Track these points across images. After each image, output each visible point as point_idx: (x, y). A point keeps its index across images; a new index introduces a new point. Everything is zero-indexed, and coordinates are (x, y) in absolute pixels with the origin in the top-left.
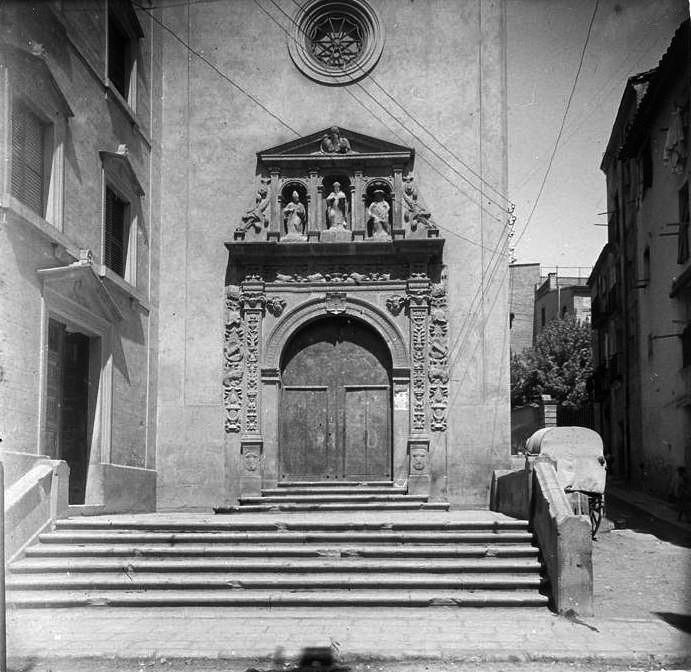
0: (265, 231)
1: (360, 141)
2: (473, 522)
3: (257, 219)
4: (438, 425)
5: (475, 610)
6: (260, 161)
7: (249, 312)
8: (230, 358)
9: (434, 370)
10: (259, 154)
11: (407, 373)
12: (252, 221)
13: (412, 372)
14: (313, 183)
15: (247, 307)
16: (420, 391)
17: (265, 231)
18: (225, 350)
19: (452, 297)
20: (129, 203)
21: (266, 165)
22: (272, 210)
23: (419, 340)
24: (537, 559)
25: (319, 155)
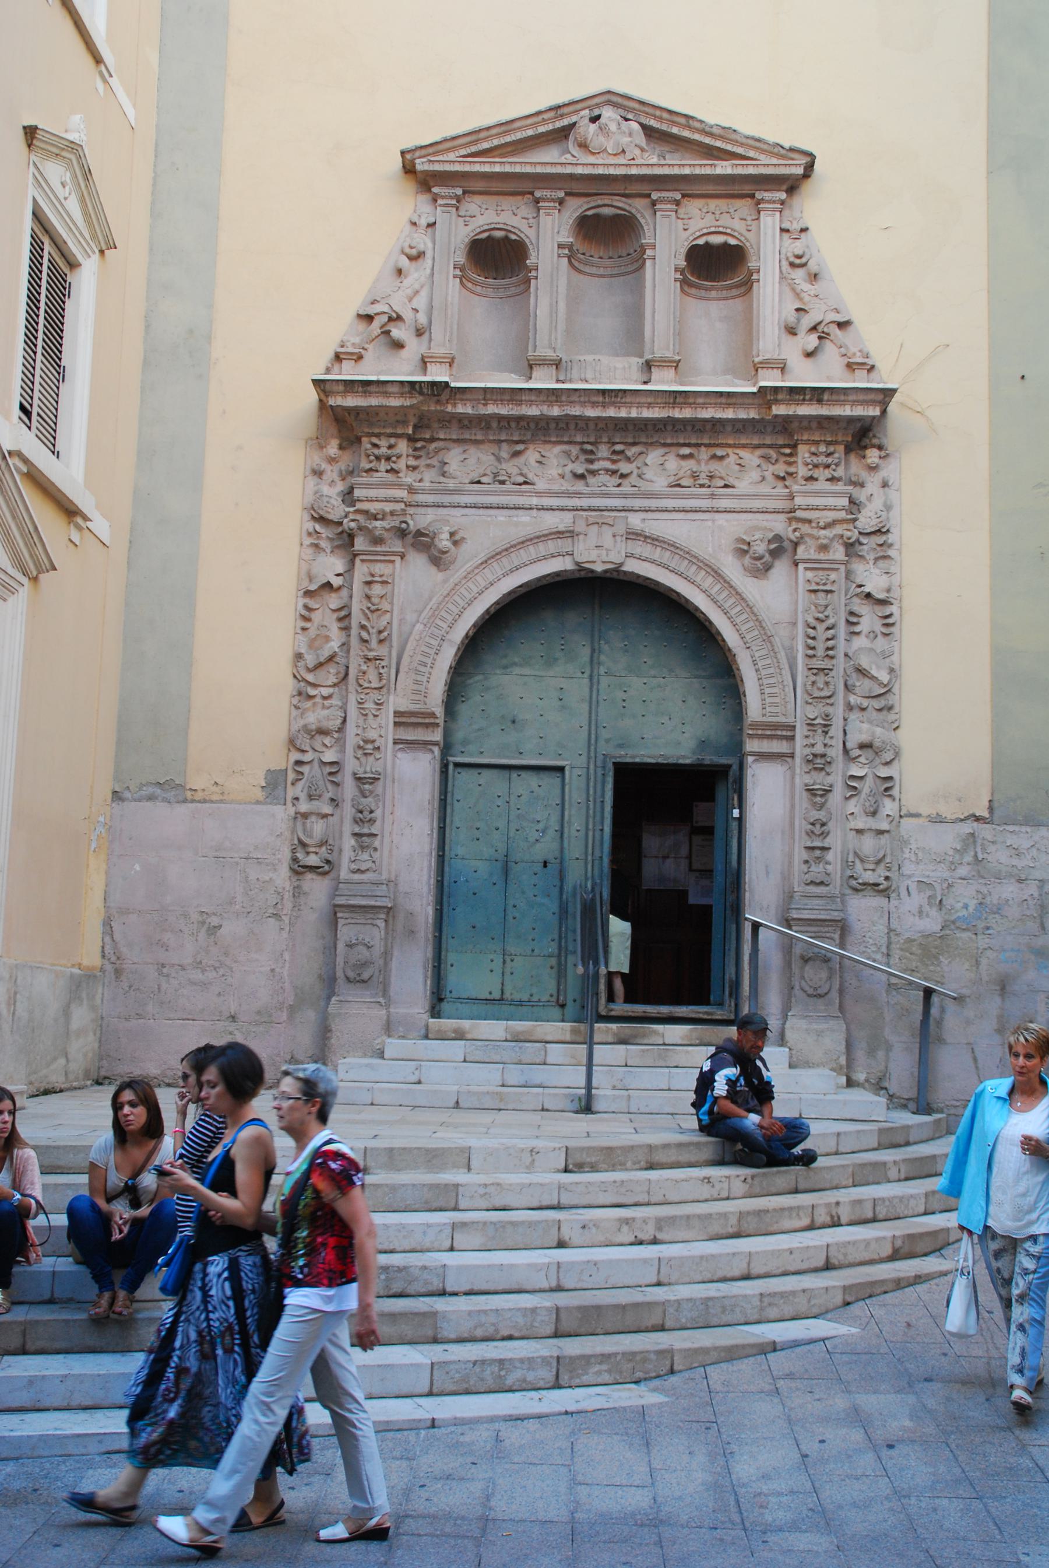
0: (414, 348)
1: (663, 130)
2: (22, 315)
3: (396, 319)
4: (869, 877)
5: (921, 1180)
6: (409, 169)
7: (371, 558)
8: (310, 677)
9: (861, 730)
10: (403, 153)
11: (786, 731)
12: (381, 325)
13: (800, 732)
14: (548, 233)
15: (360, 544)
16: (818, 780)
17: (414, 348)
18: (299, 656)
19: (910, 536)
20: (80, 265)
21: (422, 174)
22: (440, 292)
23: (820, 652)
24: (761, 1054)
25: (547, 159)
